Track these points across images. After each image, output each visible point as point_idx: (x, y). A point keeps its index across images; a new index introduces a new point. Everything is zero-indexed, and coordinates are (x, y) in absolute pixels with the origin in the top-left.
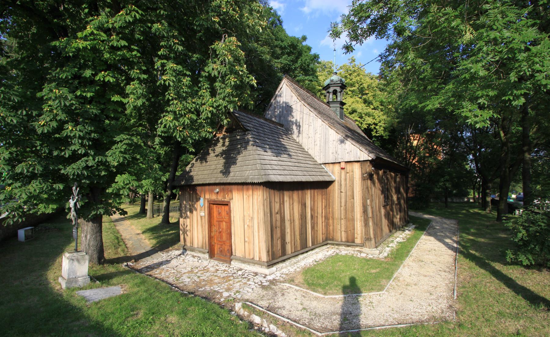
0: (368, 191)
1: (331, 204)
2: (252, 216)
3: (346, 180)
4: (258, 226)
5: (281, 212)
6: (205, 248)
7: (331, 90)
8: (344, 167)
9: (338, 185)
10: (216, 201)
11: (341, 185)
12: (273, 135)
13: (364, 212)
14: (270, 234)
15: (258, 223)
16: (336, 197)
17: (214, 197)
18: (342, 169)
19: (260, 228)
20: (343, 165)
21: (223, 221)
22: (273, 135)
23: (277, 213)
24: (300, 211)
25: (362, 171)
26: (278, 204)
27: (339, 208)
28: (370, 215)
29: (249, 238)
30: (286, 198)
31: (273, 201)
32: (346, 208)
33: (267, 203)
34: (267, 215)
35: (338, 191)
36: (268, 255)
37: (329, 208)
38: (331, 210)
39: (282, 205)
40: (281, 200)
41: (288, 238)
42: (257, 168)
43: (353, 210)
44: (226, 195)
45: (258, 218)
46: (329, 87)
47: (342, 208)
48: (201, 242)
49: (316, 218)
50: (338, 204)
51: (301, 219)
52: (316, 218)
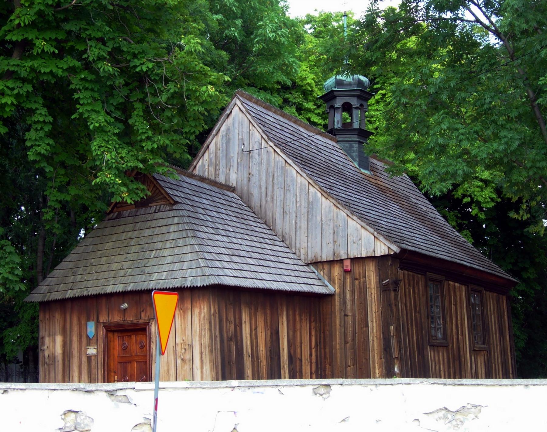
0: (392, 310)
1: (327, 340)
2: (190, 343)
3: (353, 292)
5: (237, 337)
7: (339, 103)
8: (349, 268)
9: (340, 302)
10: (122, 326)
11: (345, 302)
12: (218, 210)
13: (385, 349)
15: (201, 353)
16: (338, 327)
17: (116, 318)
18: (346, 271)
19: (204, 359)
20: (347, 265)
21: (134, 360)
22: (218, 210)
24: (269, 345)
25: (380, 276)
26: (233, 326)
27: (343, 345)
28: (395, 354)
30: (245, 317)
31: (224, 320)
32: (354, 345)
33: (215, 320)
35: (340, 313)
37: (325, 348)
38: (327, 350)
39: (238, 328)
40: (237, 320)
42: (200, 264)
43: (366, 349)
45: (201, 345)
46: (334, 97)
47: (348, 345)
49: (298, 362)
50: (341, 339)
51: (271, 357)
52: (298, 362)
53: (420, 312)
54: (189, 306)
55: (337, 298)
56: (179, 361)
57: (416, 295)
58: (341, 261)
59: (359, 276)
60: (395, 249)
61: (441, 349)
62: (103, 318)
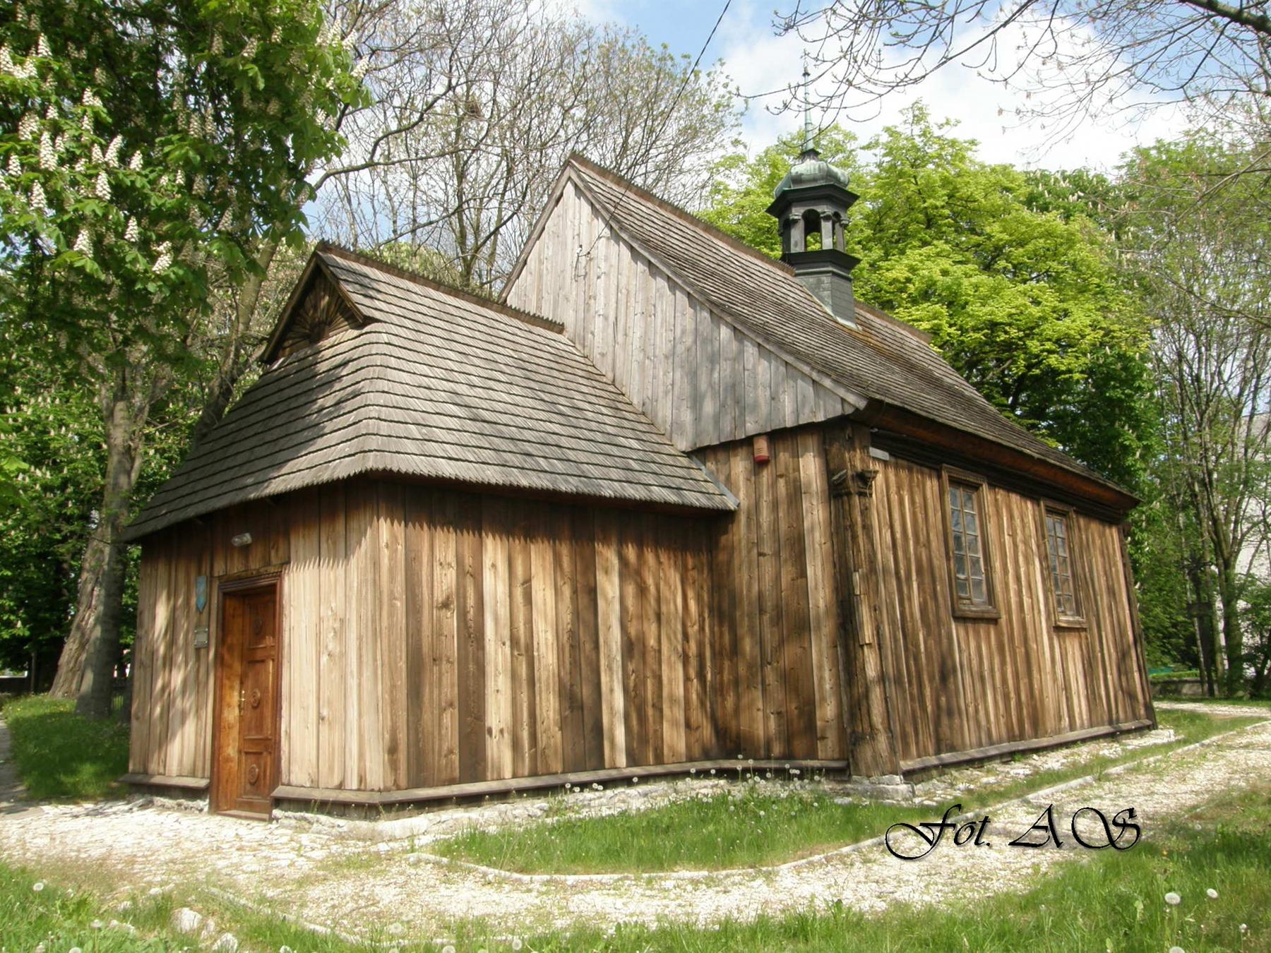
4: (360, 649)
6: (199, 773)
14: (402, 682)
15: (360, 638)
23: (446, 605)
29: (330, 703)
31: (425, 559)
34: (392, 606)
36: (394, 765)
41: (498, 712)
44: (273, 553)
47: (766, 618)
48: (192, 749)
53: (928, 545)
54: (342, 532)
55: (743, 518)
56: (324, 658)
57: (918, 510)
58: (749, 441)
59: (787, 469)
60: (856, 401)
61: (982, 628)
62: (219, 569)
